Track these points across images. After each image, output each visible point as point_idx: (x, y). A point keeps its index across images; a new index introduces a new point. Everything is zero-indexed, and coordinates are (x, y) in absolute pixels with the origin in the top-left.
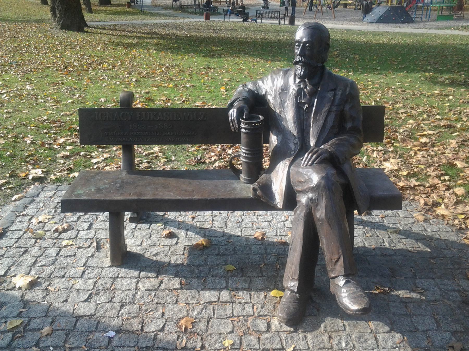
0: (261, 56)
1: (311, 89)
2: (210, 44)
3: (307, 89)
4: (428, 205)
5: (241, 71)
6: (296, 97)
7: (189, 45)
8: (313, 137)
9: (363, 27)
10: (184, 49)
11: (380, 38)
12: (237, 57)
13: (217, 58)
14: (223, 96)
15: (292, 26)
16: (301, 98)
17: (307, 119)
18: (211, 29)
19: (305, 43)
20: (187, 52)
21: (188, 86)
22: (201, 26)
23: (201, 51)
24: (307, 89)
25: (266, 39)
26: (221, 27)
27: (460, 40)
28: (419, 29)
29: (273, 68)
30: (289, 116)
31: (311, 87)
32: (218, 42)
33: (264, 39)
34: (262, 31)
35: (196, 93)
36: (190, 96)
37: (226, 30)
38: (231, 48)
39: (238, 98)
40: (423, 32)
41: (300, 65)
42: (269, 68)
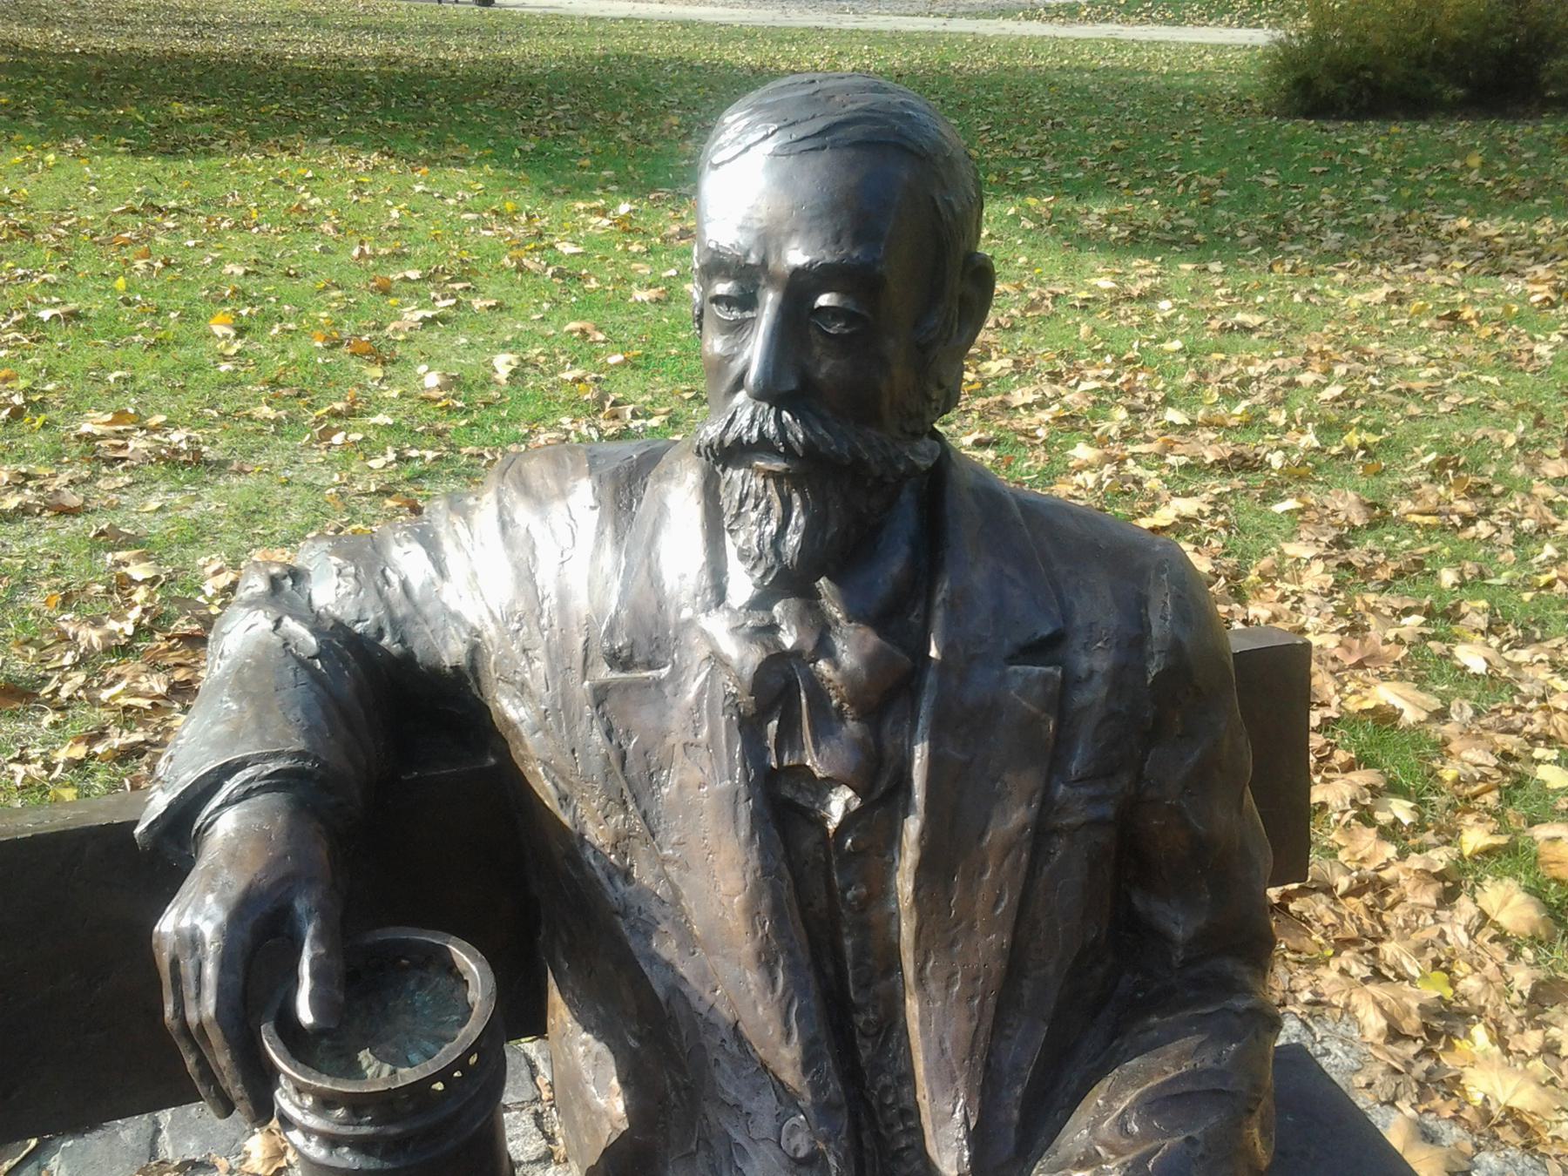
0: (383, 140)
1: (873, 662)
2: (162, 91)
3: (836, 665)
4: (1407, 1037)
5: (306, 221)
6: (749, 727)
7: (67, 96)
8: (944, 1079)
9: (735, 11)
10: (40, 117)
11: (800, 51)
12: (283, 149)
13: (195, 155)
14: (225, 367)
15: (486, 11)
16: (788, 735)
17: (865, 903)
18: (176, 23)
19: (799, 287)
20: (54, 131)
21: (46, 314)
22: (135, 11)
23: (120, 127)
24: (836, 665)
25: (397, 62)
26: (216, 12)
27: (1053, 55)
28: (918, 19)
29: (442, 198)
30: (703, 886)
31: (872, 639)
32: (199, 79)
33: (388, 60)
34: (376, 30)
35: (86, 357)
36: (51, 374)
37: (238, 25)
38: (256, 106)
39: (227, 771)
40: (932, 28)
41: (768, 475)
42: (426, 199)
